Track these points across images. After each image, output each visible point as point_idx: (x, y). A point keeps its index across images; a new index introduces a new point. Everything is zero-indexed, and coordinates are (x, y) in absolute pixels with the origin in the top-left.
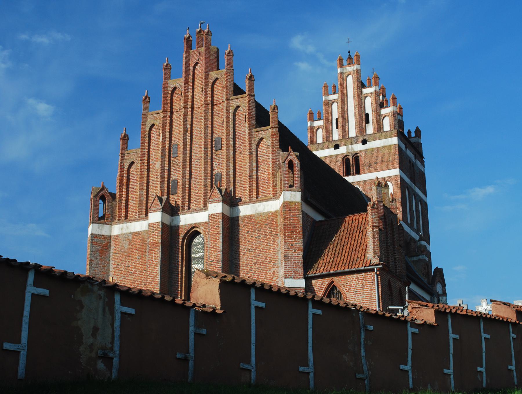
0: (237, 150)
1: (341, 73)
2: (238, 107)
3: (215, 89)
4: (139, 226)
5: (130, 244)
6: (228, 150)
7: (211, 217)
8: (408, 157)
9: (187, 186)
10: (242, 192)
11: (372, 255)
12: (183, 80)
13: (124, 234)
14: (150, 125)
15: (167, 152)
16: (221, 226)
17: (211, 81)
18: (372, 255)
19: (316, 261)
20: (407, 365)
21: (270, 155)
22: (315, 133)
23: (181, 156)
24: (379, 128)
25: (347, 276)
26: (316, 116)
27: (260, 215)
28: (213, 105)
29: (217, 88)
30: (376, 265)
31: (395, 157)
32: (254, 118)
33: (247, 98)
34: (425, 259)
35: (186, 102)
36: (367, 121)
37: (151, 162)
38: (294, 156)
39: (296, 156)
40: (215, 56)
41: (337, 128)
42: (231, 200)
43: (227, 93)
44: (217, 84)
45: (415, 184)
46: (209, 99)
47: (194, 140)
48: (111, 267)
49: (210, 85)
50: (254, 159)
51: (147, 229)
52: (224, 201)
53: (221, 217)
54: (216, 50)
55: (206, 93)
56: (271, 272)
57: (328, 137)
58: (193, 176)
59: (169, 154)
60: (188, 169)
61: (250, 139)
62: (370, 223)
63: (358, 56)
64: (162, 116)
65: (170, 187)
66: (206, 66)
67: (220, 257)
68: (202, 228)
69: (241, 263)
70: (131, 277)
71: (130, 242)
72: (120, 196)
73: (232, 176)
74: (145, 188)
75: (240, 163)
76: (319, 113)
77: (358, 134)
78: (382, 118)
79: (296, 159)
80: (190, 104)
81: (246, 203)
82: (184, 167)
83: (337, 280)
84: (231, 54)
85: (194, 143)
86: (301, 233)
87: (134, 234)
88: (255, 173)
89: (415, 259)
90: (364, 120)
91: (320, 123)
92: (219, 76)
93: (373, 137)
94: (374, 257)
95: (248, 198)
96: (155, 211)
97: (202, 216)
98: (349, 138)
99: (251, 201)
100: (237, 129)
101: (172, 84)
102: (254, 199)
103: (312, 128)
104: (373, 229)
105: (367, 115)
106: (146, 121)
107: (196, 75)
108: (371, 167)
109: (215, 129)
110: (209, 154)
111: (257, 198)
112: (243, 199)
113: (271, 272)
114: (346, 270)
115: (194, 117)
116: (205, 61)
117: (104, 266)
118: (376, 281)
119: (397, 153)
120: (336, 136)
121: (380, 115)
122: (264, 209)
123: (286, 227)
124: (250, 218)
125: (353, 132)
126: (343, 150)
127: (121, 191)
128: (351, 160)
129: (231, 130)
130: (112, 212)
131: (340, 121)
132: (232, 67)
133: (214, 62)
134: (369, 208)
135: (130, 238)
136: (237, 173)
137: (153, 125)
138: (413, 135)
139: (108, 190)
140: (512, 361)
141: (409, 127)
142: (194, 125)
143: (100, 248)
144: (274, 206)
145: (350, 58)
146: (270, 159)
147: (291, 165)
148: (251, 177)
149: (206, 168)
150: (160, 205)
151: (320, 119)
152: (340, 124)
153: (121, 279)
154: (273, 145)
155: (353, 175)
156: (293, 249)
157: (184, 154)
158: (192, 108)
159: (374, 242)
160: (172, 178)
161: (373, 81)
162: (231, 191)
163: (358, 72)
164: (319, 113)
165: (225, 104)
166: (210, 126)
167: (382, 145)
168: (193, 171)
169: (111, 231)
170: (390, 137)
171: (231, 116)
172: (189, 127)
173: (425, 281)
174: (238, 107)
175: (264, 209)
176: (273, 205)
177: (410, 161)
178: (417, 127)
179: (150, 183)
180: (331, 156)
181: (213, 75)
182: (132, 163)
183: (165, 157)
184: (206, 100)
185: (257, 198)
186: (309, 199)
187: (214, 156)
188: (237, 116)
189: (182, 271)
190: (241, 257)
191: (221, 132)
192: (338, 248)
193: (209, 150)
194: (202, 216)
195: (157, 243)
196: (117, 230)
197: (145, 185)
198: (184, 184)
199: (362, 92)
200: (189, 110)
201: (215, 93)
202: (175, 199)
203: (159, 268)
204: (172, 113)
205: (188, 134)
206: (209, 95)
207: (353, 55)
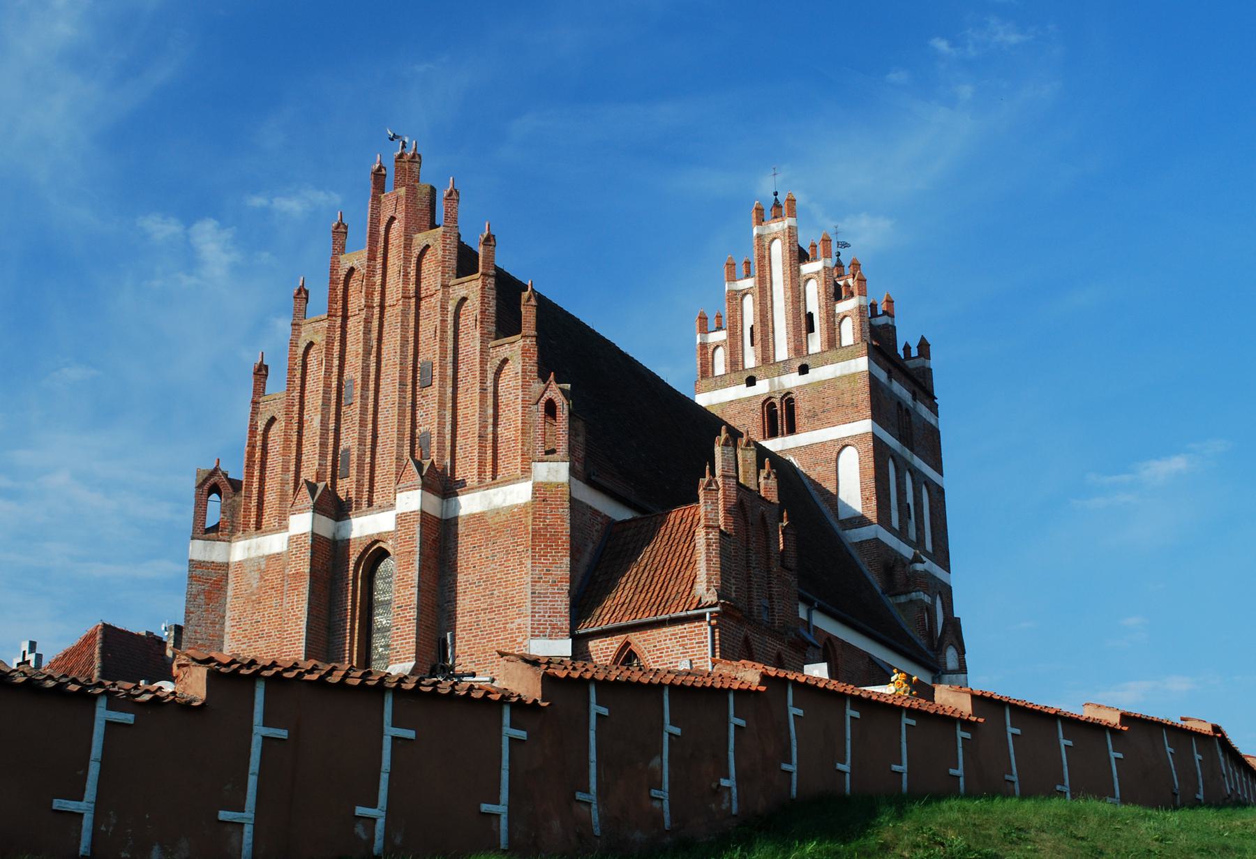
0: (460, 385)
1: (759, 236)
2: (464, 299)
3: (424, 267)
4: (275, 543)
5: (262, 577)
6: (442, 386)
7: (401, 519)
8: (892, 394)
9: (368, 460)
10: (466, 470)
11: (705, 590)
12: (365, 253)
13: (251, 560)
14: (304, 345)
15: (334, 396)
16: (417, 536)
17: (416, 252)
18: (704, 585)
19: (599, 602)
20: (81, 800)
21: (520, 392)
22: (710, 356)
23: (359, 400)
24: (833, 340)
25: (655, 632)
26: (712, 323)
27: (497, 512)
28: (419, 299)
29: (429, 266)
30: (710, 606)
31: (864, 396)
32: (494, 319)
33: (480, 283)
34: (922, 601)
35: (369, 295)
36: (811, 329)
37: (306, 417)
38: (558, 391)
39: (563, 391)
40: (427, 203)
41: (752, 344)
42: (443, 484)
43: (443, 273)
44: (427, 256)
45: (912, 450)
46: (412, 287)
47: (383, 369)
48: (227, 624)
49: (414, 260)
50: (490, 401)
51: (285, 548)
52: (426, 487)
53: (418, 518)
54: (429, 189)
55: (406, 274)
56: (514, 626)
57: (735, 363)
58: (380, 440)
59: (338, 397)
60: (370, 426)
61: (483, 362)
62: (702, 521)
63: (792, 201)
64: (326, 324)
65: (338, 467)
66: (407, 223)
67: (415, 598)
68: (390, 542)
69: (459, 610)
70: (261, 644)
71: (263, 574)
72: (249, 484)
73: (448, 437)
74: (293, 468)
75: (465, 411)
76: (719, 317)
77: (792, 355)
78: (838, 320)
79: (562, 397)
80: (377, 299)
81: (472, 489)
82: (363, 423)
83: (635, 638)
84: (454, 196)
85: (383, 376)
86: (567, 546)
87: (269, 558)
88: (490, 429)
89: (903, 599)
90: (804, 326)
91: (721, 336)
92: (430, 242)
94: (708, 590)
95: (476, 479)
96: (301, 511)
97: (388, 517)
98: (775, 363)
99: (482, 485)
100: (461, 344)
101: (346, 262)
102: (489, 480)
103: (704, 346)
104: (707, 534)
105: (810, 317)
106: (298, 336)
107: (391, 241)
108: (819, 419)
109: (422, 347)
110: (409, 395)
111: (494, 478)
112: (469, 482)
113: (514, 626)
114: (651, 618)
115: (386, 323)
116: (407, 213)
117: (213, 623)
118: (709, 639)
119: (867, 389)
120: (751, 359)
122: (504, 501)
123: (535, 534)
124: (479, 519)
125: (782, 352)
126: (762, 387)
127: (250, 475)
128: (778, 406)
129: (450, 345)
130: (233, 516)
132: (456, 221)
133: (426, 213)
134: (701, 492)
135: (263, 567)
136: (460, 432)
137: (311, 344)
138: (914, 353)
139: (226, 475)
140: (499, 793)
141: (906, 336)
142: (385, 340)
143: (206, 587)
144: (519, 494)
145: (777, 205)
146: (520, 400)
147: (551, 409)
148: (482, 437)
149: (401, 423)
150: (310, 498)
151: (719, 328)
152: (758, 337)
153: (244, 646)
154: (524, 371)
155: (783, 435)
156: (550, 579)
157: (364, 397)
158: (382, 307)
159: (708, 560)
160: (343, 445)
161: (820, 249)
162: (445, 468)
163: (792, 233)
164: (719, 317)
165: (440, 295)
166: (411, 340)
167: (838, 374)
168: (380, 430)
169: (229, 554)
170: (853, 357)
171: (450, 318)
172: (375, 343)
173: (923, 643)
174: (464, 299)
175: (504, 501)
176: (518, 490)
177: (899, 404)
178: (923, 338)
179: (304, 458)
180: (739, 401)
181: (420, 239)
182: (272, 420)
183: (329, 405)
184: (405, 289)
185: (494, 478)
186: (593, 478)
187: (419, 398)
188: (462, 318)
189: (352, 628)
190: (460, 598)
191: (430, 352)
192: (645, 575)
193: (409, 388)
194: (388, 517)
195: (302, 575)
196: (240, 550)
197: (293, 462)
198: (361, 458)
199: (799, 270)
200: (376, 310)
201: (423, 275)
202: (345, 487)
203: (303, 624)
204: (345, 318)
205: (373, 358)
206: (413, 279)
207: (782, 198)
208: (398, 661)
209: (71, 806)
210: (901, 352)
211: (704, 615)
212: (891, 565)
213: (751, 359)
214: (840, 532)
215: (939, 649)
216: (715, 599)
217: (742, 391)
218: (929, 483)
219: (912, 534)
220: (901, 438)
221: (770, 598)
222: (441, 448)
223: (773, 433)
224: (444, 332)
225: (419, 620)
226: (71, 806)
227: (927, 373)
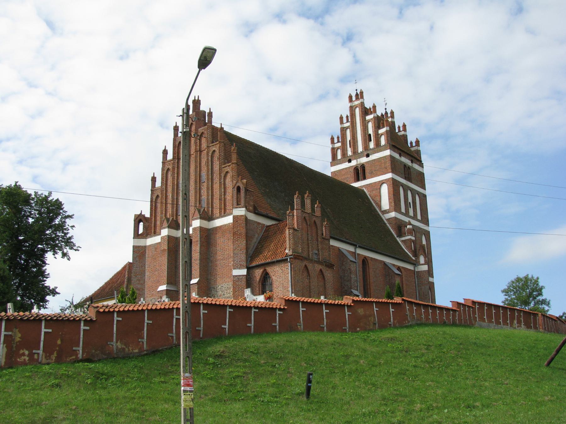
2: (214, 151)
24: (378, 144)
31: (388, 164)
46: (198, 147)
57: (344, 154)
67: (199, 256)
93: (375, 151)
96: (164, 228)
105: (370, 135)
117: (142, 267)
120: (350, 153)
121: (378, 134)
125: (360, 149)
126: (354, 163)
131: (351, 141)
138: (414, 144)
144: (228, 220)
145: (357, 95)
147: (239, 189)
151: (338, 142)
152: (352, 144)
159: (289, 240)
180: (346, 169)
181: (200, 130)
210: (409, 145)
211: (287, 259)
212: (400, 227)
213: (350, 153)
214: (381, 214)
216: (291, 253)
217: (346, 165)
218: (419, 193)
219: (411, 213)
220: (406, 178)
221: (318, 250)
222: (208, 204)
223: (358, 180)
224: (208, 163)
225: (200, 264)
227: (418, 152)
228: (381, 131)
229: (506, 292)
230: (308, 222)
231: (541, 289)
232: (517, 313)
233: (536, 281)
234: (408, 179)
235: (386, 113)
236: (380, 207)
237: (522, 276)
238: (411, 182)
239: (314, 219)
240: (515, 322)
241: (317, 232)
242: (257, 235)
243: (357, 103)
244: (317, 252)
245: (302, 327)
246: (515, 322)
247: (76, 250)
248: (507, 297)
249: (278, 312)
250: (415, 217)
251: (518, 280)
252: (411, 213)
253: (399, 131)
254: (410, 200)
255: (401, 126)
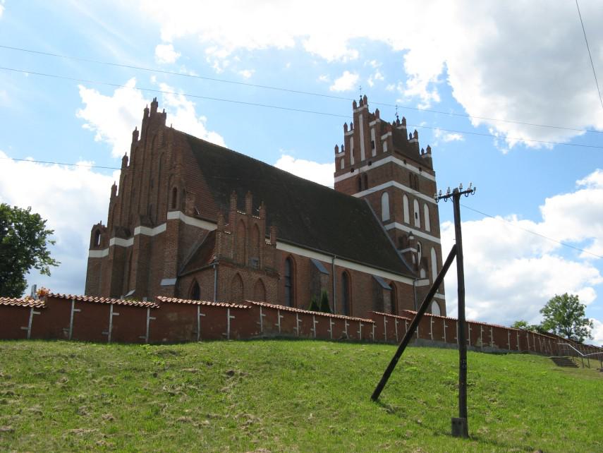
57: (347, 163)
93: (377, 159)
120: (353, 162)
125: (363, 158)
126: (356, 172)
138: (425, 152)
208: (452, 313)
209: (77, 310)
214: (382, 226)
215: (417, 269)
217: (349, 175)
218: (429, 204)
220: (411, 187)
221: (259, 257)
226: (77, 310)
228: (384, 137)
229: (546, 311)
230: (246, 225)
231: (582, 309)
232: (484, 329)
233: (576, 299)
234: (415, 187)
235: (398, 121)
236: (380, 217)
237: (560, 294)
238: (418, 191)
239: (256, 222)
240: (480, 340)
241: (259, 236)
242: (196, 242)
243: (360, 109)
244: (257, 259)
245: (71, 333)
246: (480, 340)
247: (55, 265)
248: (546, 317)
249: (32, 312)
250: (422, 229)
251: (558, 299)
252: (417, 223)
253: (411, 138)
254: (416, 209)
255: (413, 133)
